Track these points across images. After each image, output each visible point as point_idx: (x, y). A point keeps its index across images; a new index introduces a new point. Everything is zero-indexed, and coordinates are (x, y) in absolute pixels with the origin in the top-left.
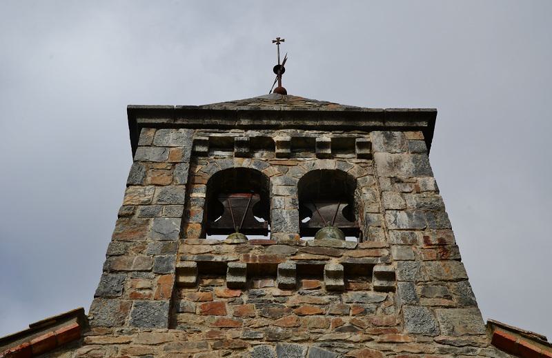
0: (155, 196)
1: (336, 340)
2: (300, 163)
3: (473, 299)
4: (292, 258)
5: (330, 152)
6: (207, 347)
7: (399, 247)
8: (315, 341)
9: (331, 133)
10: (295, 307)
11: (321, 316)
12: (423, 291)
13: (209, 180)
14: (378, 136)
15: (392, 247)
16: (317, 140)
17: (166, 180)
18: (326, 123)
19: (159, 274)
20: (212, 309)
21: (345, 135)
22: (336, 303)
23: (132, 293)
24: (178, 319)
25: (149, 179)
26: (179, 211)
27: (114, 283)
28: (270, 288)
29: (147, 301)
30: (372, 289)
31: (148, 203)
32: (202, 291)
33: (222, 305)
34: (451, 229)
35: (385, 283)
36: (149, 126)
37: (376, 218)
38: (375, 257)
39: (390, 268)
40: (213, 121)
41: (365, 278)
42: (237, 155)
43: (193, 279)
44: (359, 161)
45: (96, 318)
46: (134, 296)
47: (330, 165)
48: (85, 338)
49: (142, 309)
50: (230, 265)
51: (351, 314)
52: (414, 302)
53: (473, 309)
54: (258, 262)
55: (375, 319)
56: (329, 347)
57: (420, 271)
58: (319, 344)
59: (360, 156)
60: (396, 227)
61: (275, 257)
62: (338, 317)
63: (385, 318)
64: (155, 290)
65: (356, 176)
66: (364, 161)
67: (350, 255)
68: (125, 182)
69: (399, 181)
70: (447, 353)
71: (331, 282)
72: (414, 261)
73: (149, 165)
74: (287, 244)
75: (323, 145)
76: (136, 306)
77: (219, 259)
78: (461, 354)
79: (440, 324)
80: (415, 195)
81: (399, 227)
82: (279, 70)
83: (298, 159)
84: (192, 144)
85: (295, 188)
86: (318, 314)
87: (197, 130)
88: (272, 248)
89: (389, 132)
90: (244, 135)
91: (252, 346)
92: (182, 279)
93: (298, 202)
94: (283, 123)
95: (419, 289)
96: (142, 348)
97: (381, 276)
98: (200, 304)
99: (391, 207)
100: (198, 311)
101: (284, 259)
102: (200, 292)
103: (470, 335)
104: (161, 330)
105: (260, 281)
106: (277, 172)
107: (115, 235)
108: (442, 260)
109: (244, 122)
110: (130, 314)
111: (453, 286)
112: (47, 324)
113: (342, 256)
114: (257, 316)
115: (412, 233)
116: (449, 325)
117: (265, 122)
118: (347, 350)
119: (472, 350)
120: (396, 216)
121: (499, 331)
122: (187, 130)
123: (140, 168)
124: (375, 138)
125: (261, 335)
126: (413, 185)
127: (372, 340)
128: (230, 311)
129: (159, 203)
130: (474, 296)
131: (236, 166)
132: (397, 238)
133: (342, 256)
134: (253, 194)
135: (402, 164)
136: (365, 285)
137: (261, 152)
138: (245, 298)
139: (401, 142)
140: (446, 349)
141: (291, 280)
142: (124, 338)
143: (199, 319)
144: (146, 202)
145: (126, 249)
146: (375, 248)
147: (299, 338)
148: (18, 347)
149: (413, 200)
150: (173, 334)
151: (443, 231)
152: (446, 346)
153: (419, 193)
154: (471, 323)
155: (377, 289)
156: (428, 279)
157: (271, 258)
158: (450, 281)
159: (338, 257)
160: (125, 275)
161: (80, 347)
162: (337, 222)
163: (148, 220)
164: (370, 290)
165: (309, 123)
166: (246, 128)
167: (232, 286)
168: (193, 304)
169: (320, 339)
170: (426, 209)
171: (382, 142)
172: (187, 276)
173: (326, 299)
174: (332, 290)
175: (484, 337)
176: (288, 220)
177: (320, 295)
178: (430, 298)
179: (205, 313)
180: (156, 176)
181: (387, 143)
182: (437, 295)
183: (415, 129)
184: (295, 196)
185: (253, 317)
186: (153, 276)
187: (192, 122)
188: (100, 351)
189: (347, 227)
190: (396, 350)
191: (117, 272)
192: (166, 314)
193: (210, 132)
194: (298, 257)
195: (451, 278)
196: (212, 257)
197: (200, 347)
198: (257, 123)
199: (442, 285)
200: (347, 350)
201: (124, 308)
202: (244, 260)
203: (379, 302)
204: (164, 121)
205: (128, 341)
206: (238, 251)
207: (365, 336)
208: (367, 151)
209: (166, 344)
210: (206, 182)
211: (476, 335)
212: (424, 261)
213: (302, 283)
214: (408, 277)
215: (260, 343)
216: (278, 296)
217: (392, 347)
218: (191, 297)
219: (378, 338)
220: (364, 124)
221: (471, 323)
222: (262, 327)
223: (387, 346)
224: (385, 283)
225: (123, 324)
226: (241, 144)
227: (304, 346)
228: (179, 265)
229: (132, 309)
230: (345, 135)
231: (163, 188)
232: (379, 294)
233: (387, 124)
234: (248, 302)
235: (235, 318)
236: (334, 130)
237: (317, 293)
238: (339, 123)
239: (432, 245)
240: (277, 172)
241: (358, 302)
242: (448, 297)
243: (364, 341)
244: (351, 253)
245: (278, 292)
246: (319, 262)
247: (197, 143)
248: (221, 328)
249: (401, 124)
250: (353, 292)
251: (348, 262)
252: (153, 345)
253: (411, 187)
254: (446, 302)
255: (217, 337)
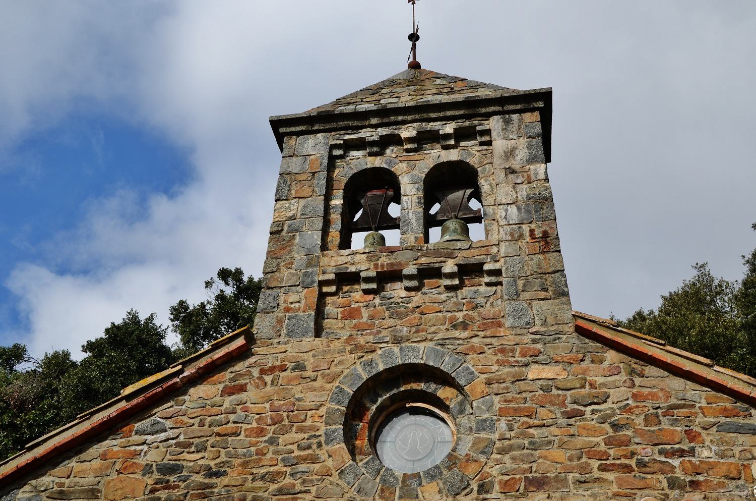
0: (299, 210)
1: (448, 339)
2: (428, 156)
3: (566, 289)
4: (414, 262)
5: (453, 143)
6: (345, 352)
7: (507, 243)
8: (431, 340)
9: (454, 123)
10: (418, 307)
11: (440, 314)
12: (524, 286)
13: (347, 185)
14: (498, 121)
15: (501, 244)
16: (441, 132)
17: (307, 191)
18: (449, 113)
19: (306, 288)
20: (351, 314)
21: (467, 124)
22: (451, 299)
23: (285, 308)
24: (324, 325)
25: (293, 192)
26: (319, 224)
27: (271, 299)
28: (397, 290)
29: (297, 314)
30: (484, 284)
31: (293, 218)
32: (342, 298)
33: (358, 310)
34: (555, 219)
35: (493, 279)
36: (291, 134)
37: (491, 211)
38: (485, 255)
39: (497, 266)
40: (346, 123)
41: (477, 274)
42: (370, 154)
43: (333, 289)
44: (480, 148)
45: (259, 332)
46: (287, 310)
47: (453, 155)
48: (253, 350)
49: (293, 321)
50: (363, 274)
51: (464, 310)
52: (515, 297)
53: (565, 299)
54: (385, 269)
55: (484, 313)
56: (442, 345)
57: (523, 266)
58: (434, 343)
59: (481, 144)
60: (506, 223)
61: (400, 264)
62: (453, 314)
63: (492, 311)
64: (303, 302)
65: (476, 166)
66: (485, 147)
67: (464, 255)
68: (274, 198)
69: (513, 172)
70: (538, 343)
71: (448, 282)
72: (519, 256)
73: (293, 177)
74: (411, 250)
75: (447, 137)
76: (289, 319)
77: (353, 269)
78: (549, 342)
79: (535, 316)
80: (526, 186)
81: (508, 222)
82: (414, 37)
83: (425, 152)
84: (328, 150)
85: (421, 185)
86: (437, 312)
87: (333, 133)
88: (397, 255)
89: (507, 116)
90: (374, 134)
91: (381, 348)
92: (325, 289)
93: (423, 201)
94: (409, 118)
95: (520, 283)
96: (296, 356)
97: (491, 273)
98: (341, 310)
99: (503, 201)
100: (340, 316)
101: (407, 264)
102: (340, 299)
103: (559, 324)
104: (309, 340)
105: (389, 284)
106: (405, 169)
107: (269, 252)
108: (544, 253)
109: (374, 121)
110: (285, 327)
111: (550, 278)
112: (221, 343)
113: (457, 257)
114: (387, 318)
115: (520, 227)
116: (543, 317)
117: (392, 118)
118: (457, 347)
119: (559, 338)
120: (506, 211)
121: (581, 323)
122: (323, 134)
123: (285, 182)
124: (494, 124)
125: (388, 339)
126: (525, 174)
127: (478, 336)
128: (365, 313)
129: (302, 217)
130: (567, 286)
131: (369, 166)
132: (506, 234)
133: (457, 257)
134: (387, 189)
135: (517, 152)
136: (477, 280)
137: (391, 148)
138: (377, 301)
139: (519, 126)
140: (537, 339)
141: (414, 283)
142: (282, 348)
143: (340, 325)
144: (292, 217)
145: (278, 265)
146: (486, 246)
147: (418, 339)
148: (205, 363)
149: (524, 191)
150: (319, 342)
151: (547, 222)
152: (538, 337)
153: (530, 183)
154: (560, 313)
155: (488, 284)
156: (529, 274)
157: (397, 265)
158: (548, 273)
159: (454, 258)
160: (279, 290)
161: (249, 357)
162: (461, 211)
163: (294, 235)
164: (482, 285)
165: (433, 115)
166: (376, 126)
167: (367, 292)
168: (335, 310)
169: (435, 339)
170: (535, 200)
171: (500, 128)
172: (328, 286)
173: (443, 297)
174: (449, 288)
175: (570, 325)
176: (413, 221)
177: (439, 293)
178: (529, 291)
179: (344, 318)
180: (299, 188)
181: (505, 129)
182: (535, 288)
183: (532, 110)
184: (421, 194)
185: (384, 319)
186: (301, 290)
187: (327, 126)
188: (264, 361)
189: (470, 216)
190: (496, 344)
191: (272, 288)
192: (312, 325)
193: (344, 134)
194: (419, 261)
195: (549, 271)
196: (347, 268)
197: (340, 352)
198: (386, 120)
199: (541, 279)
200: (457, 347)
201: (280, 321)
202: (375, 268)
203: (489, 297)
204: (303, 128)
205: (284, 351)
206: (369, 260)
207: (471, 332)
208: (487, 138)
209: (313, 352)
210: (343, 187)
211: (564, 324)
212: (528, 255)
213: (424, 283)
214: (511, 274)
215: (386, 345)
216: (405, 297)
217: (493, 340)
218: (333, 304)
219: (482, 334)
220: (483, 110)
221: (560, 313)
222: (391, 327)
223: (489, 340)
224: (493, 279)
225: (280, 335)
226: (372, 144)
227: (422, 346)
228: (321, 278)
229: (286, 322)
230: (467, 124)
231: (305, 200)
232: (489, 288)
233: (505, 108)
234: (380, 305)
235: (369, 321)
236: (456, 120)
237: (436, 292)
238: (461, 112)
239: (535, 238)
240: (405, 169)
241: (471, 298)
242: (546, 290)
243: (471, 338)
244: (465, 253)
245: (404, 293)
246: (437, 265)
247: (333, 147)
248: (358, 330)
249: (518, 107)
250: (467, 288)
251: (461, 263)
252: (304, 352)
253: (523, 177)
254: (543, 294)
255: (353, 343)
